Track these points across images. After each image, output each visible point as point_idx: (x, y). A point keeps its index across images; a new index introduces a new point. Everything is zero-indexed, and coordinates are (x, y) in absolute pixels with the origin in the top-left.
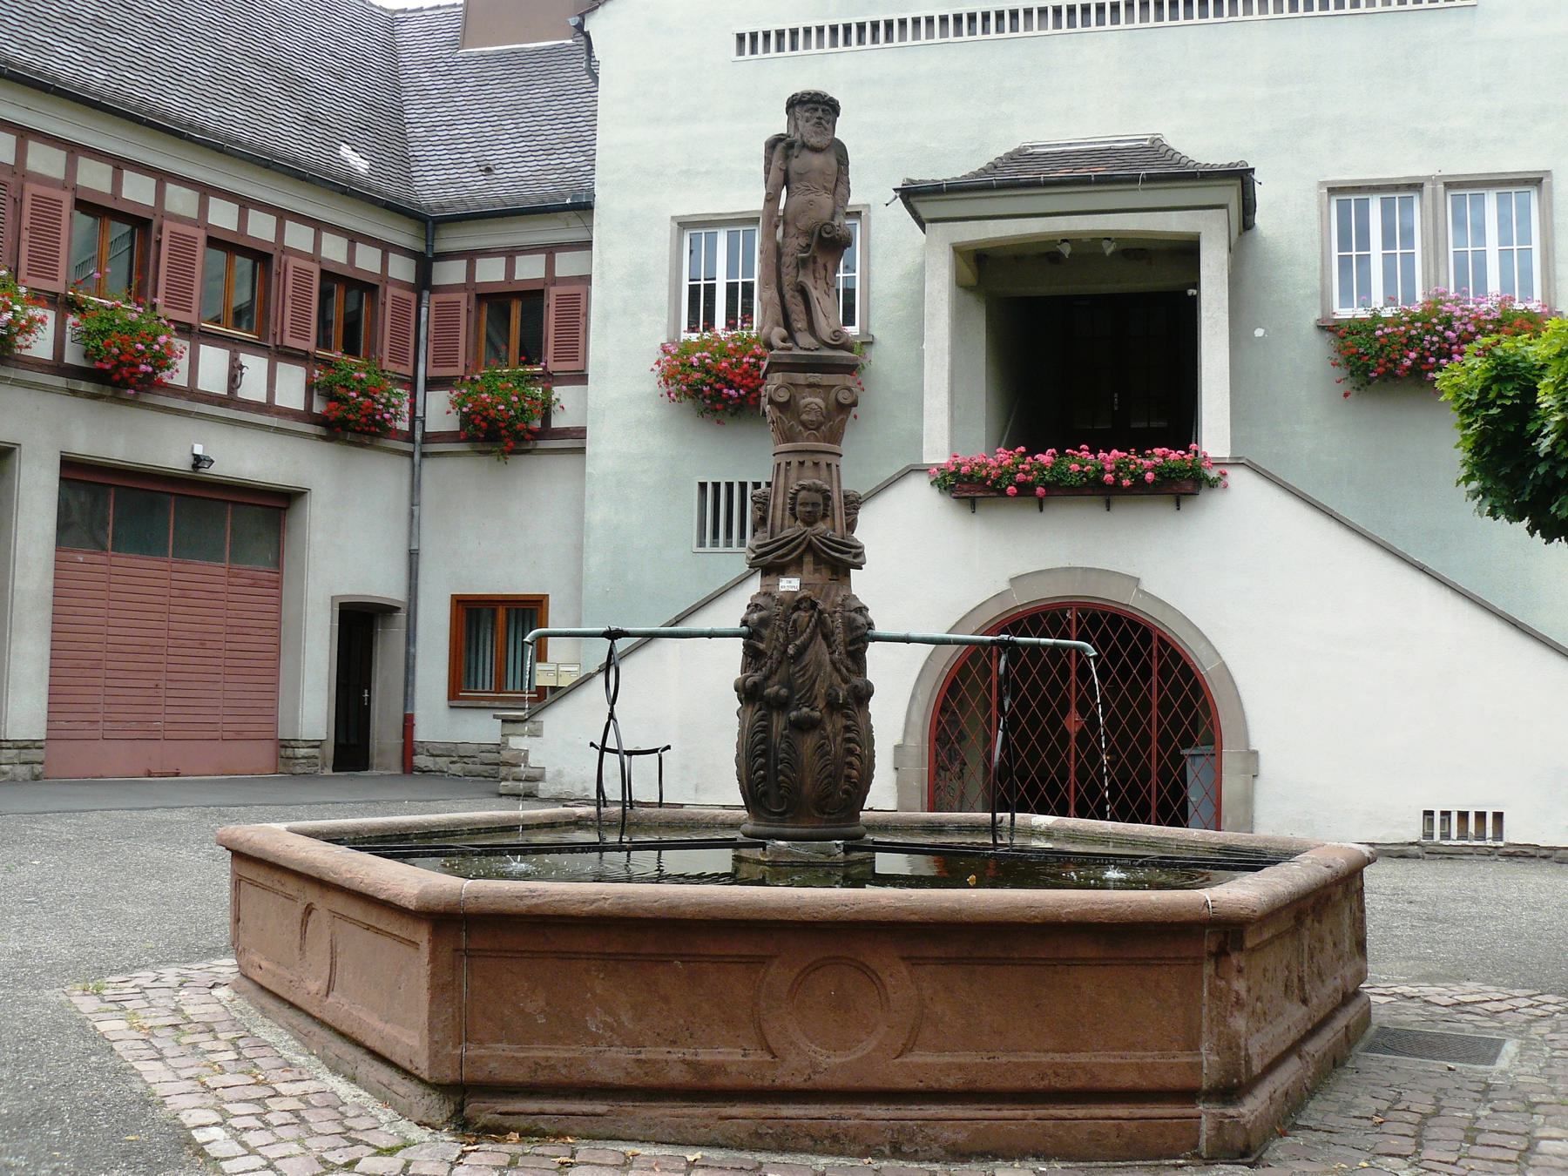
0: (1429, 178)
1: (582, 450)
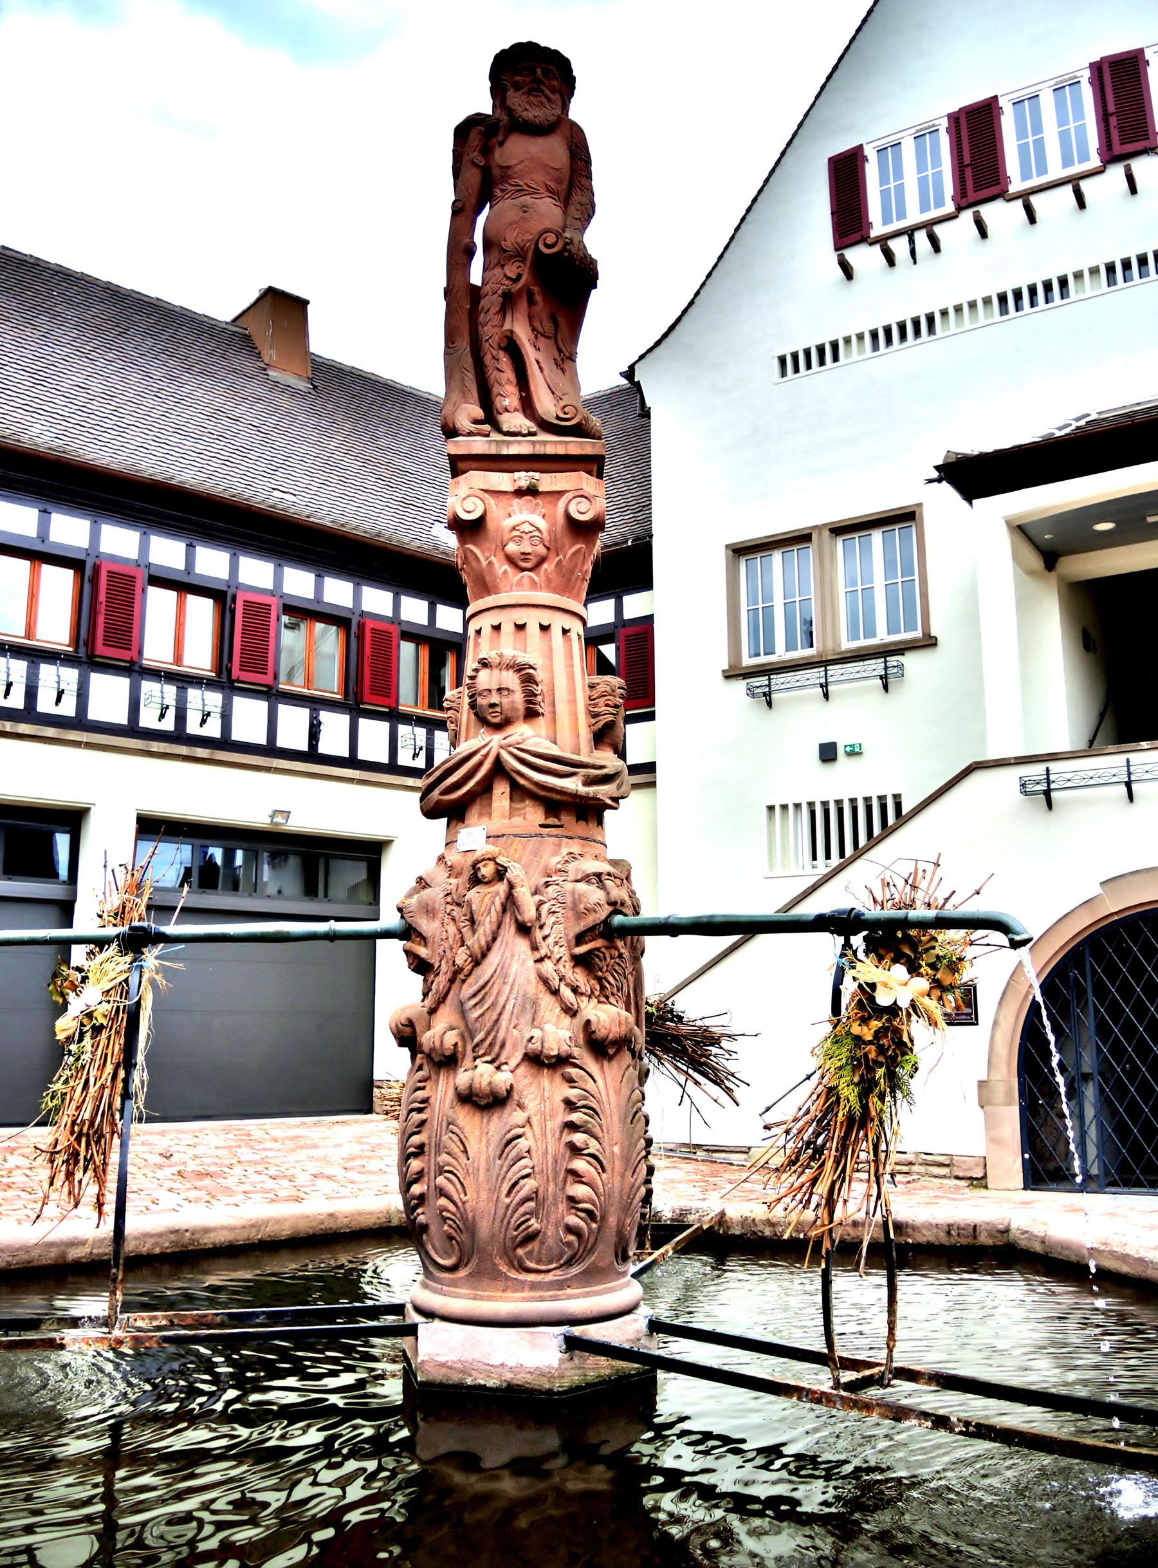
1: (652, 784)
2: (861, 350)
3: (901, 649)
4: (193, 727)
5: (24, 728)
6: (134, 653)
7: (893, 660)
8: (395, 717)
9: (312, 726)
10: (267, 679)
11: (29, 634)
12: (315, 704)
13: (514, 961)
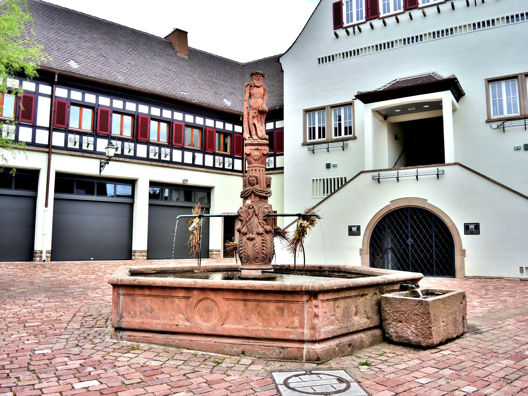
0: (519, 74)
1: (283, 173)
2: (340, 58)
3: (347, 139)
4: (163, 158)
5: (121, 159)
6: (148, 139)
7: (345, 142)
8: (214, 154)
9: (193, 157)
10: (181, 145)
11: (121, 134)
12: (194, 151)
13: (255, 220)
